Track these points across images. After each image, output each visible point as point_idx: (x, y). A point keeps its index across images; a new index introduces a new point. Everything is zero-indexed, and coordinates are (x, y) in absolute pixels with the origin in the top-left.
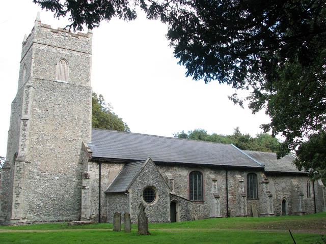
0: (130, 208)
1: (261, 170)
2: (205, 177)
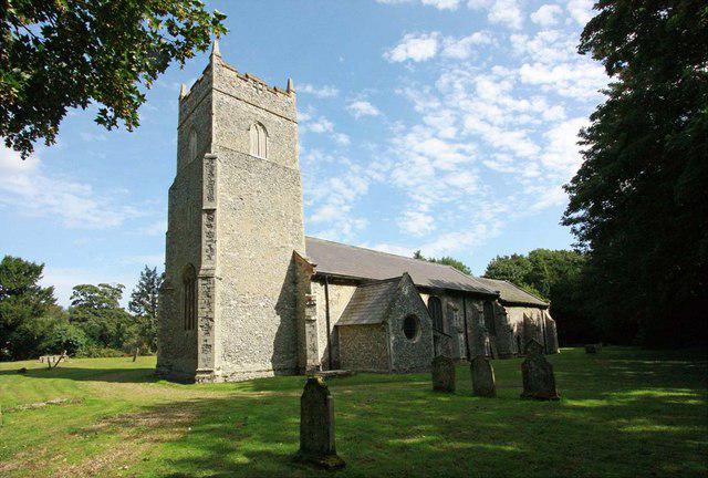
2: (444, 305)
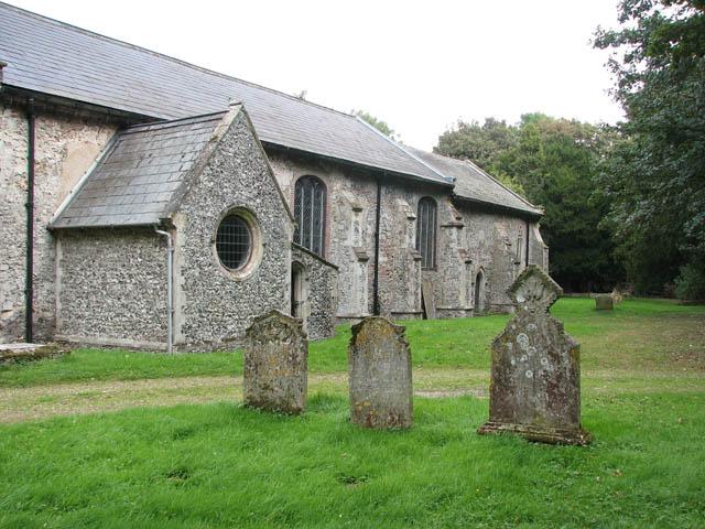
0: (178, 289)
1: (446, 190)
2: (332, 197)
